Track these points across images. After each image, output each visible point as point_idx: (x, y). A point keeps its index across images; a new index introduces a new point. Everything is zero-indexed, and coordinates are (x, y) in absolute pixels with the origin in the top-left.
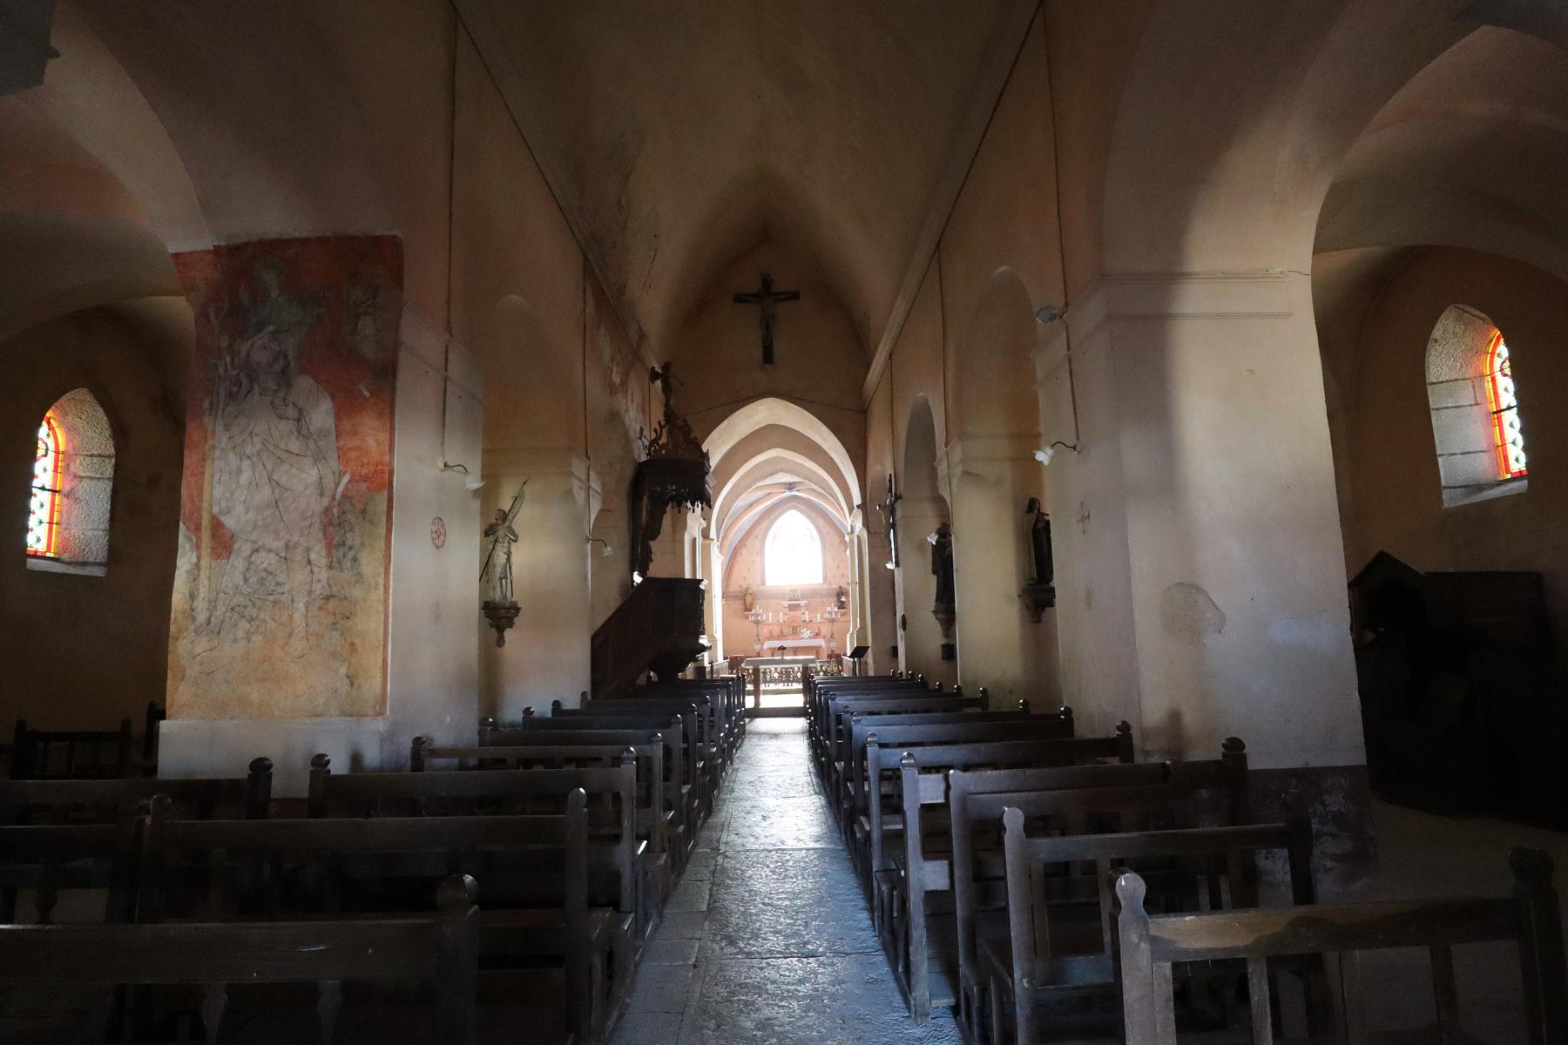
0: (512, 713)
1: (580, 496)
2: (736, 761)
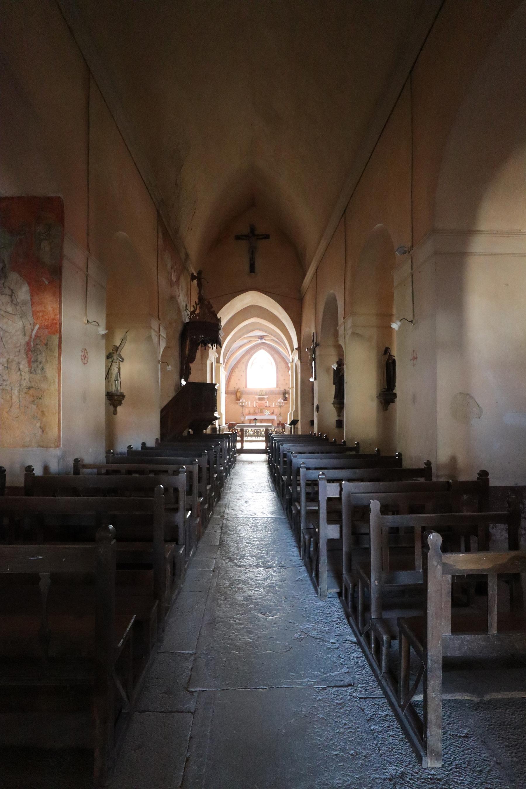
0: (121, 448)
1: (155, 339)
2: (232, 474)
